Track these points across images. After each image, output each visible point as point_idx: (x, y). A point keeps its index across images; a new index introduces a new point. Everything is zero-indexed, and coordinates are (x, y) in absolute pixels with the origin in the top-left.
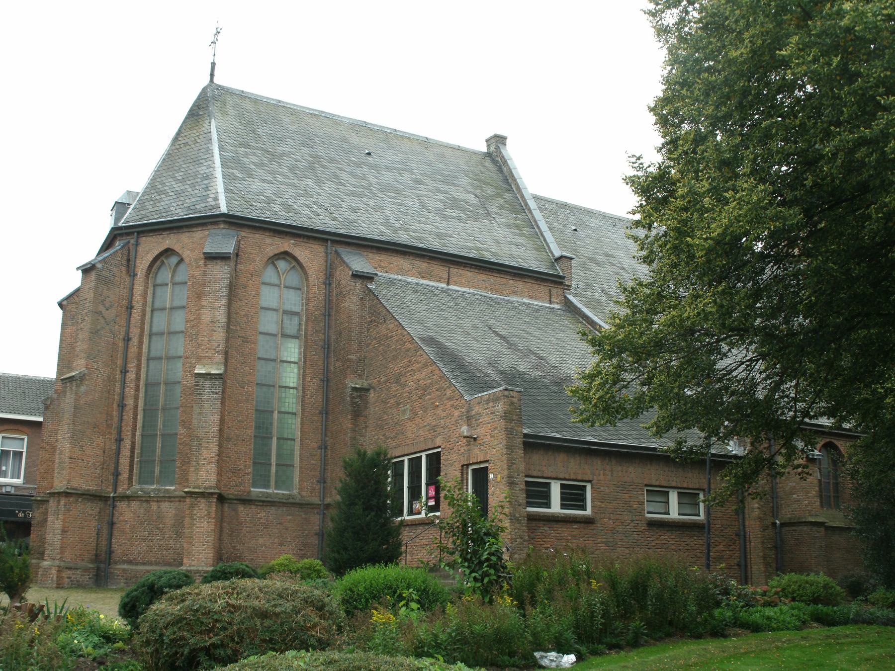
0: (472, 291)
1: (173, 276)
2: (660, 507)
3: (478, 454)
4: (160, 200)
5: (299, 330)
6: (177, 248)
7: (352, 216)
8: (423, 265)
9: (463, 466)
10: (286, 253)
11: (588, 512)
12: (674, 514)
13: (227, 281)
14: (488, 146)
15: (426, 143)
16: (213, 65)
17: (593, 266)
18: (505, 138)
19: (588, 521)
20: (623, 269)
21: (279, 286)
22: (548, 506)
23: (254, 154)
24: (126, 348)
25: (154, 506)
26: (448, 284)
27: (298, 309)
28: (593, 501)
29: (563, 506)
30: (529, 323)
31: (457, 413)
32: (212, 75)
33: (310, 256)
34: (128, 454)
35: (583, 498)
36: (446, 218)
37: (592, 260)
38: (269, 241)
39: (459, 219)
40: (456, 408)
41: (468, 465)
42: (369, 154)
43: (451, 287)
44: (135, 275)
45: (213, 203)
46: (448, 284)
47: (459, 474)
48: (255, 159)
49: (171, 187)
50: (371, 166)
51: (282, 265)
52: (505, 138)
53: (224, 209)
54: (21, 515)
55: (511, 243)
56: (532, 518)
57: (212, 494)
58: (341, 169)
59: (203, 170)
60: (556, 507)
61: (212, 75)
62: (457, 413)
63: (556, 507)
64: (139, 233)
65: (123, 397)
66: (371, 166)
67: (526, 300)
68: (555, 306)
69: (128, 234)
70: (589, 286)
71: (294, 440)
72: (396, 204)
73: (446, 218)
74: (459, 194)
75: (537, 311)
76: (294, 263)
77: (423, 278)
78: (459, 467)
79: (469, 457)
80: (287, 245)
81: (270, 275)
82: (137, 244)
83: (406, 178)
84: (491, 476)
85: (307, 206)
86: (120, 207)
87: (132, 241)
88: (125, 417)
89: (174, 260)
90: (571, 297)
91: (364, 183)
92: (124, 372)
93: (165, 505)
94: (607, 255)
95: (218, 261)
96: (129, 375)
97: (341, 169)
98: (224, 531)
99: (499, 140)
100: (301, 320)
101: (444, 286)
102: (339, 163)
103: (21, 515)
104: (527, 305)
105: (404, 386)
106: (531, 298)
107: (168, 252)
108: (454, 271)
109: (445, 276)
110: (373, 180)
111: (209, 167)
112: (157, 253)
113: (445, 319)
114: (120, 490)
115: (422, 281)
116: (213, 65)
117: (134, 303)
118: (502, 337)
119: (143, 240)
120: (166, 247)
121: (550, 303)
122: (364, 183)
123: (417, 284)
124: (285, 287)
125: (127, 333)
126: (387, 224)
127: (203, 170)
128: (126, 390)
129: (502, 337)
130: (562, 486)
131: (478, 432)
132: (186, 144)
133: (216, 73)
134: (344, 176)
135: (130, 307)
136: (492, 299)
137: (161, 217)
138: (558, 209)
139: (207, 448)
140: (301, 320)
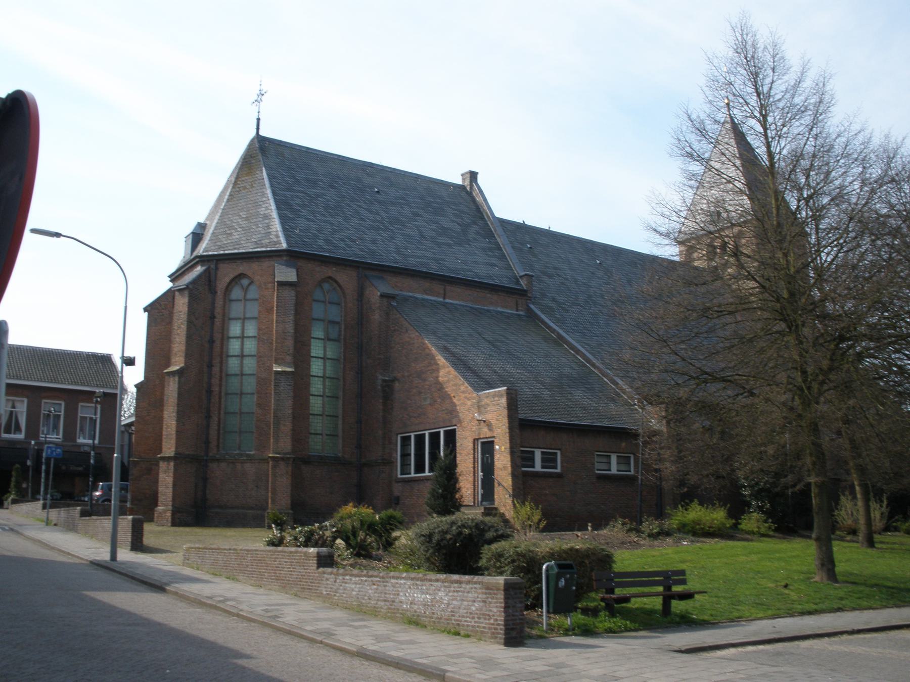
0: (461, 303)
1: (245, 294)
2: (604, 466)
3: (485, 432)
4: (231, 234)
5: (340, 335)
6: (249, 274)
7: (373, 247)
8: (427, 284)
9: (474, 440)
10: (330, 278)
11: (559, 470)
12: (614, 470)
13: (293, 302)
14: (464, 180)
15: (417, 177)
16: (258, 120)
17: (545, 279)
18: (476, 174)
19: (559, 476)
20: (567, 279)
21: (324, 302)
22: (533, 467)
23: (297, 197)
24: (211, 349)
25: (239, 466)
26: (444, 298)
27: (338, 319)
28: (562, 463)
29: (543, 467)
30: (505, 329)
31: (469, 403)
32: (258, 129)
33: (347, 278)
34: (216, 428)
35: (555, 461)
36: (439, 245)
37: (544, 273)
38: (318, 269)
39: (449, 245)
40: (469, 399)
41: (478, 439)
42: (786, 586)
43: (447, 301)
44: (216, 292)
45: (275, 240)
46: (444, 298)
47: (471, 445)
48: (298, 201)
49: (239, 224)
50: (380, 202)
51: (326, 286)
52: (476, 174)
53: (284, 246)
54: (64, 468)
55: (487, 264)
56: (525, 474)
57: (288, 458)
58: (360, 207)
59: (262, 211)
60: (538, 467)
61: (258, 129)
62: (469, 403)
63: (538, 467)
64: (217, 260)
65: (210, 385)
66: (380, 202)
67: (499, 309)
68: (521, 313)
69: (208, 261)
70: (544, 295)
71: (337, 417)
72: (403, 235)
73: (439, 245)
74: (446, 223)
75: (508, 318)
76: (335, 285)
77: (427, 294)
78: (471, 440)
79: (479, 434)
80: (331, 271)
81: (318, 294)
82: (217, 269)
83: (406, 211)
84: (497, 447)
85: (342, 240)
86: (196, 237)
87: (213, 266)
88: (213, 400)
89: (245, 282)
90: (532, 306)
91: (378, 218)
92: (210, 366)
93: (248, 466)
94: (555, 268)
95: (239, 262)
96: (214, 369)
97: (360, 207)
98: (297, 483)
99: (473, 176)
100: (340, 328)
101: (441, 300)
102: (358, 201)
103: (64, 468)
104: (501, 313)
105: (425, 380)
106: (503, 307)
107: (241, 276)
108: (448, 288)
109: (442, 292)
110: (384, 214)
111: (267, 209)
112: (232, 276)
113: (450, 329)
114: (211, 454)
115: (426, 297)
116: (258, 120)
117: (216, 315)
118: (489, 342)
119: (221, 265)
120: (240, 272)
121: (517, 310)
122: (378, 218)
123: (423, 299)
124: (330, 303)
125: (212, 337)
126: (398, 252)
127: (262, 211)
128: (213, 380)
129: (489, 342)
130: (542, 453)
131: (488, 417)
132: (245, 188)
133: (261, 127)
134: (362, 211)
135: (213, 317)
136: (475, 309)
137: (235, 249)
138: (519, 232)
139: (284, 425)
140: (340, 328)
